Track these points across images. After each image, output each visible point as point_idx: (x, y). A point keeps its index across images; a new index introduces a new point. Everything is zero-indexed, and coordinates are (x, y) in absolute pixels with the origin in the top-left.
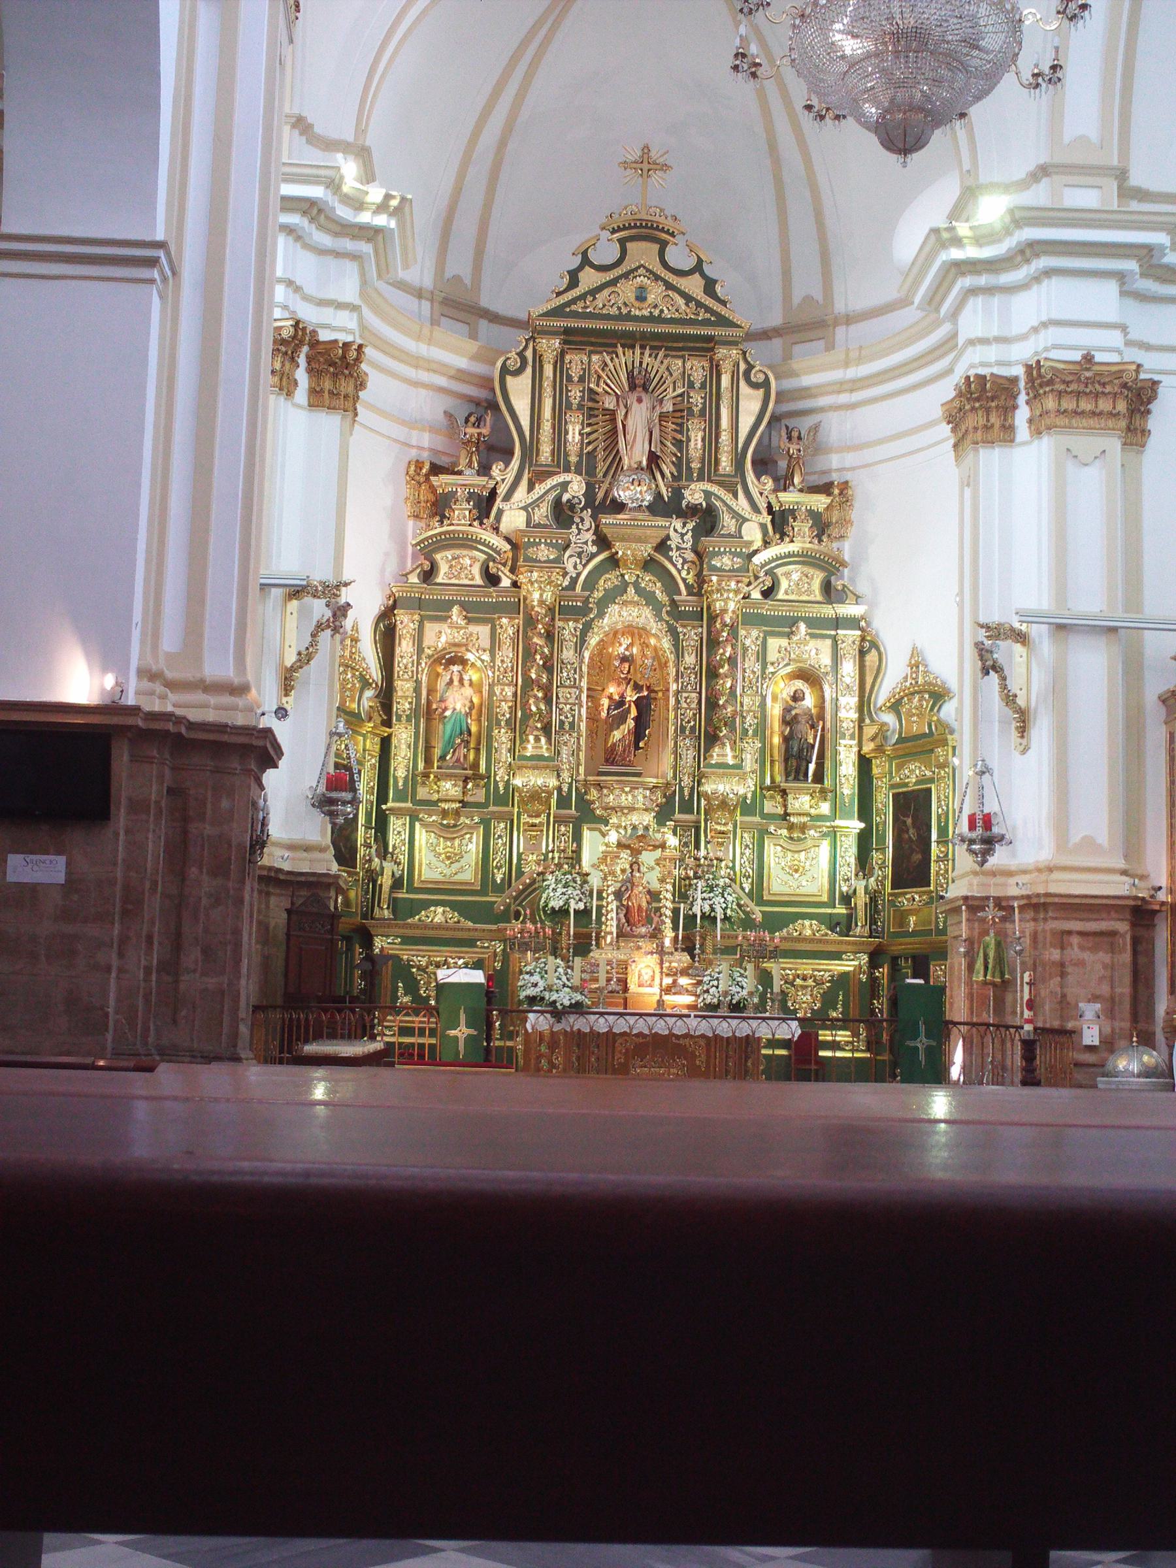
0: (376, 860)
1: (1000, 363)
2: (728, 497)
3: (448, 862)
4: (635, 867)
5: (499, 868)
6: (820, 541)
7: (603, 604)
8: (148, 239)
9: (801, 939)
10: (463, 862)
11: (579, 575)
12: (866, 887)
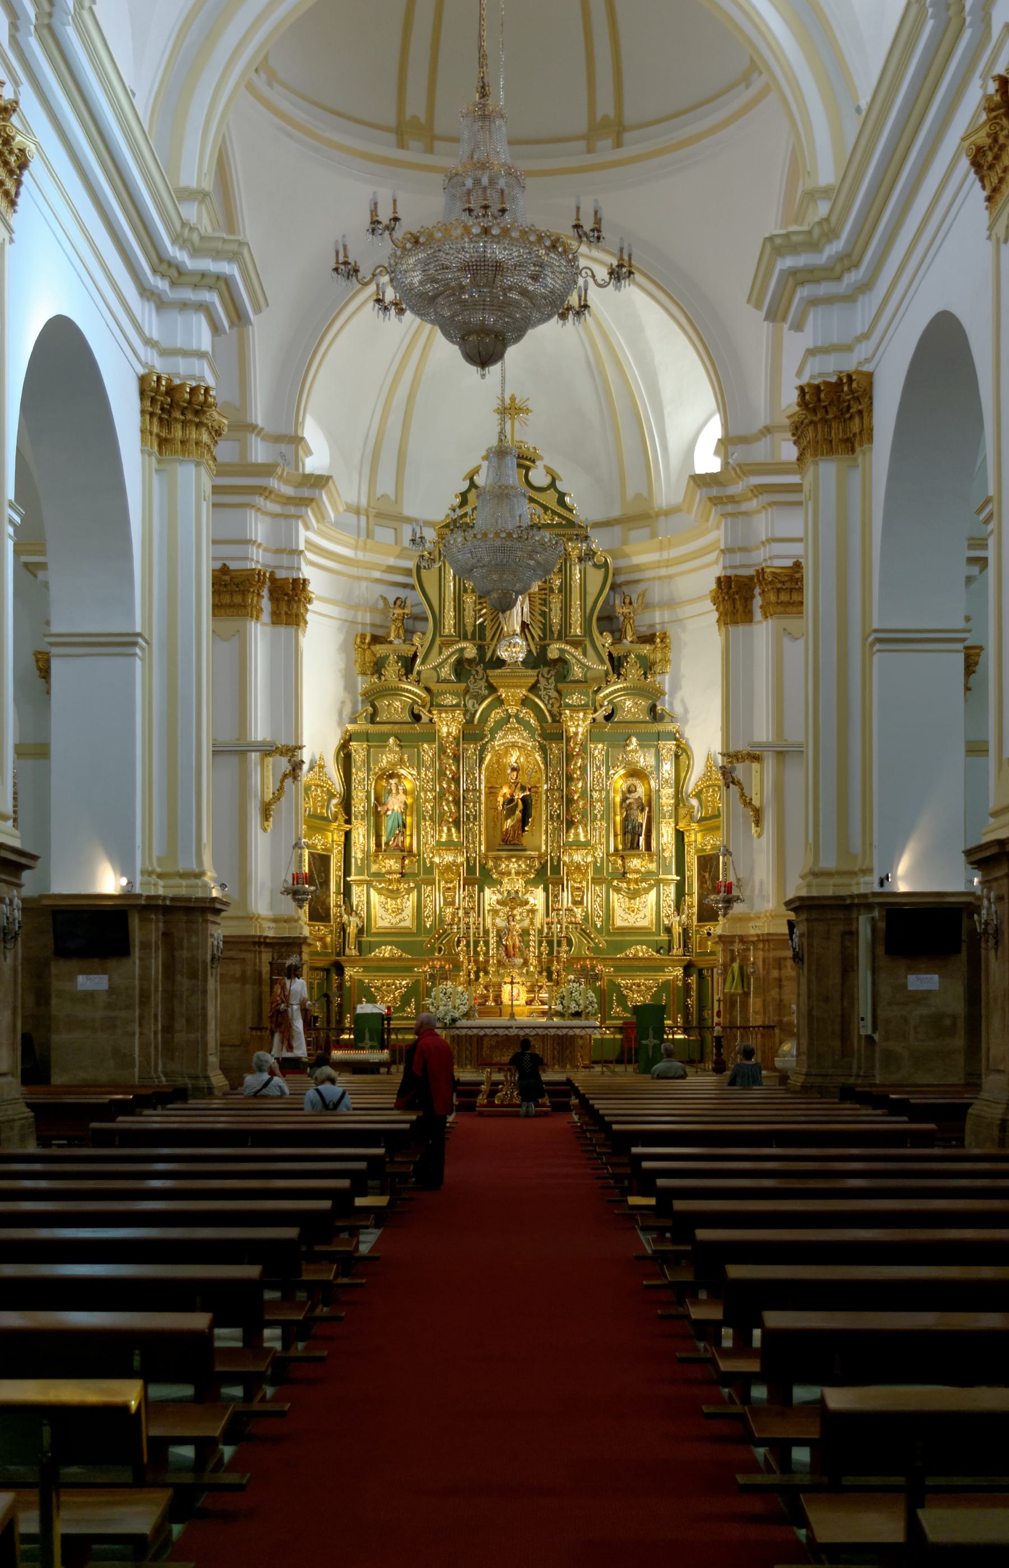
0: (345, 916)
2: (578, 653)
3: (394, 915)
4: (511, 918)
5: (428, 917)
6: (646, 678)
7: (493, 732)
8: (130, 632)
9: (636, 958)
10: (404, 914)
11: (476, 711)
12: (679, 922)
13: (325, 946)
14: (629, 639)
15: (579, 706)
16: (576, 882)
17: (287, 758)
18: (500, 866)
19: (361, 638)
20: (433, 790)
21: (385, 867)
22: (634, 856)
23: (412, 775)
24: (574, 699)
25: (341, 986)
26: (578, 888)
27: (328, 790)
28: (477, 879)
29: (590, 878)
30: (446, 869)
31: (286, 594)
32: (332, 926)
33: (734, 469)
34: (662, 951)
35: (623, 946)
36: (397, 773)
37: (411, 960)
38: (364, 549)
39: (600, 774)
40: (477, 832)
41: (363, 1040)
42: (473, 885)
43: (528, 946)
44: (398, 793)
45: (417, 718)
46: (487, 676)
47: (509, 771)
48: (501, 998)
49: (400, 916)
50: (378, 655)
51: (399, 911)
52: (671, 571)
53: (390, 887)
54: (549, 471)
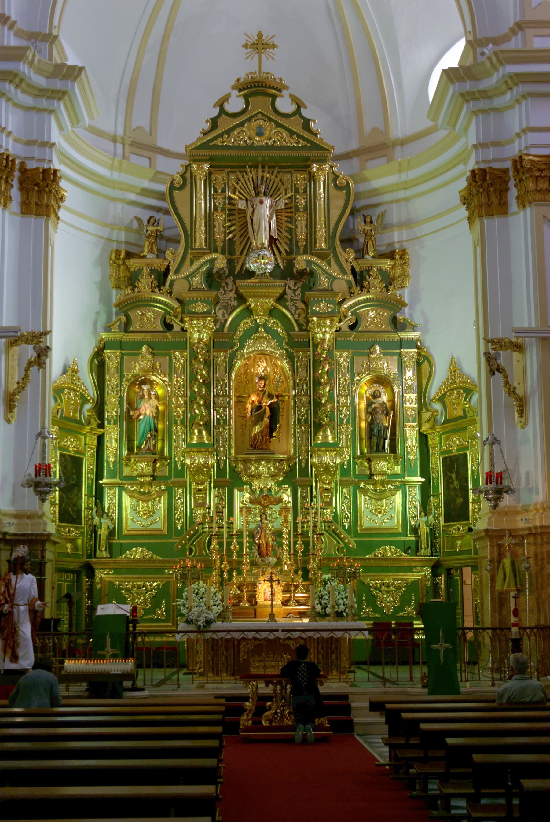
0: (97, 518)
1: (495, 160)
5: (179, 519)
6: (388, 290)
7: (243, 341)
9: (385, 558)
10: (155, 517)
11: (226, 321)
12: (427, 522)
13: (75, 548)
14: (371, 254)
15: (326, 313)
16: (324, 483)
17: (33, 346)
18: (250, 468)
19: (116, 254)
20: (184, 396)
21: (137, 470)
22: (380, 458)
23: (164, 381)
24: (321, 307)
25: (91, 589)
26: (327, 489)
27: (81, 394)
28: (227, 481)
29: (338, 479)
30: (197, 471)
31: (37, 185)
32: (83, 528)
33: (489, 59)
34: (409, 551)
35: (371, 547)
36: (149, 379)
37: (163, 562)
38: (120, 170)
39: (346, 380)
40: (227, 436)
41: (103, 647)
42: (223, 487)
43: (281, 545)
44: (150, 398)
45: (168, 327)
46: (237, 288)
47: (257, 380)
48: (256, 599)
49: (151, 519)
50: (132, 269)
51: (150, 513)
52: (409, 193)
53: (142, 490)
54: (295, 99)
